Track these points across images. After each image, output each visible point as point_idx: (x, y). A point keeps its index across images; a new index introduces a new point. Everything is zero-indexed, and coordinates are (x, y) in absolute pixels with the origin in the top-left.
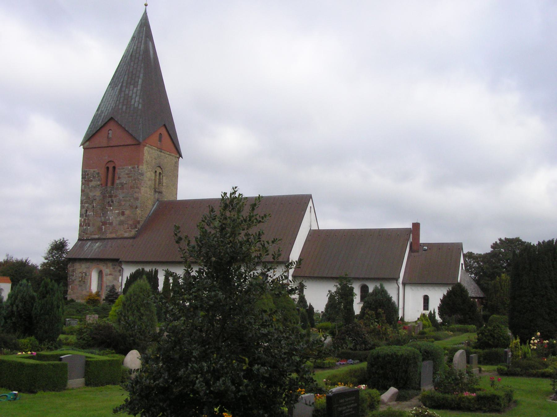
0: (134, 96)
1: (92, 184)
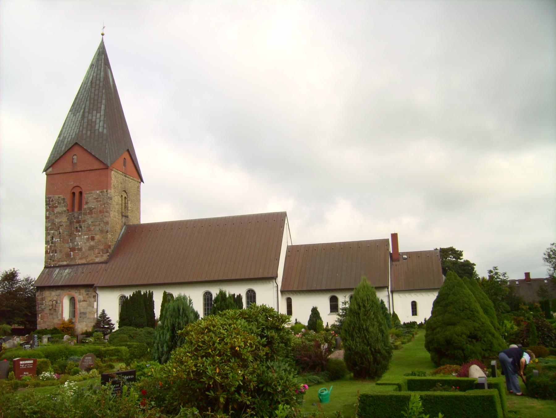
0: (98, 121)
1: (56, 210)
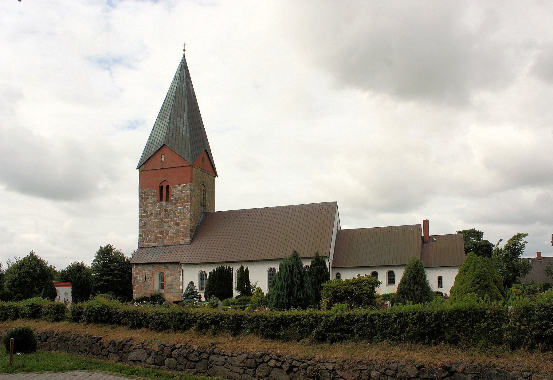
0: (182, 125)
